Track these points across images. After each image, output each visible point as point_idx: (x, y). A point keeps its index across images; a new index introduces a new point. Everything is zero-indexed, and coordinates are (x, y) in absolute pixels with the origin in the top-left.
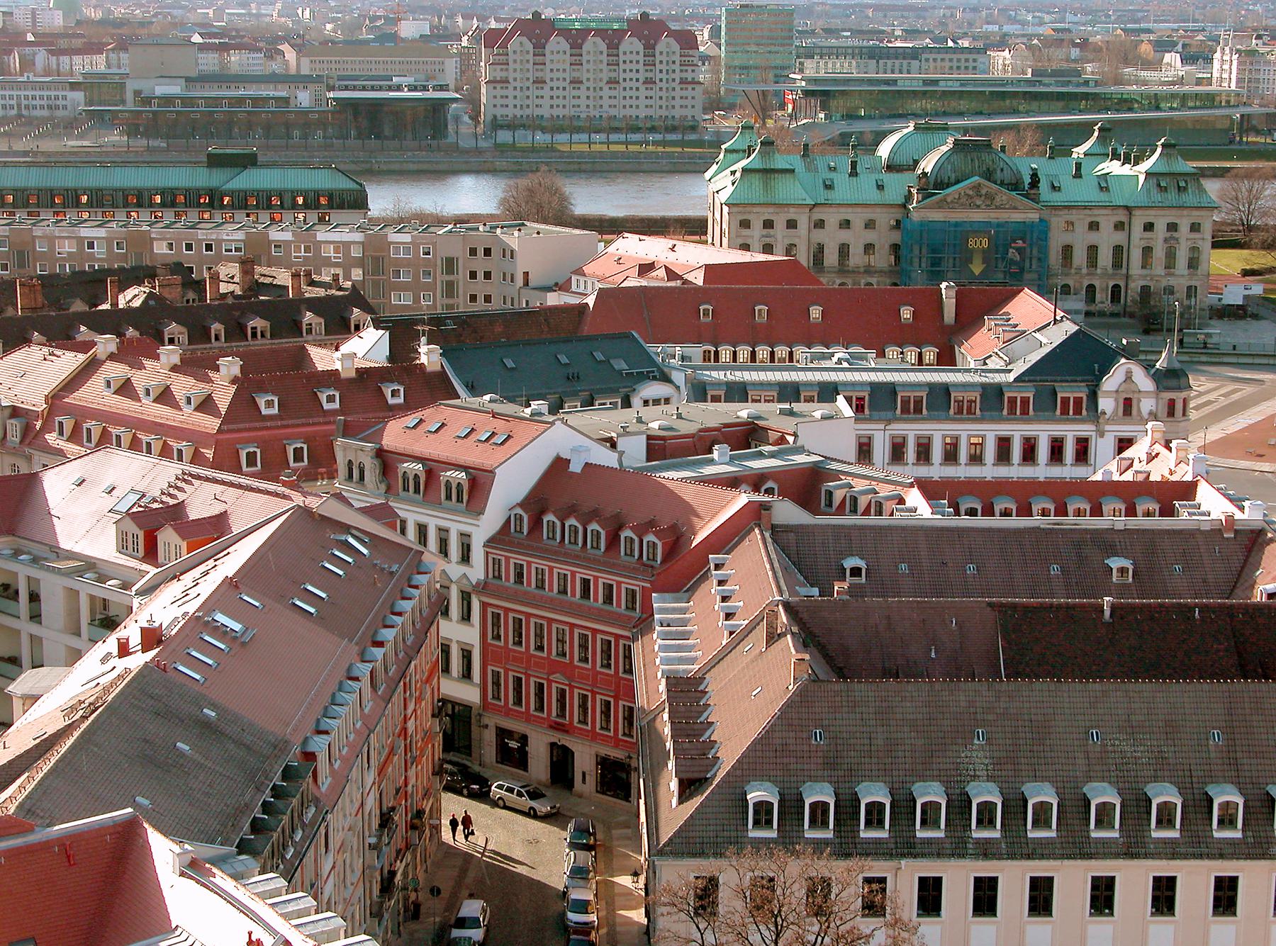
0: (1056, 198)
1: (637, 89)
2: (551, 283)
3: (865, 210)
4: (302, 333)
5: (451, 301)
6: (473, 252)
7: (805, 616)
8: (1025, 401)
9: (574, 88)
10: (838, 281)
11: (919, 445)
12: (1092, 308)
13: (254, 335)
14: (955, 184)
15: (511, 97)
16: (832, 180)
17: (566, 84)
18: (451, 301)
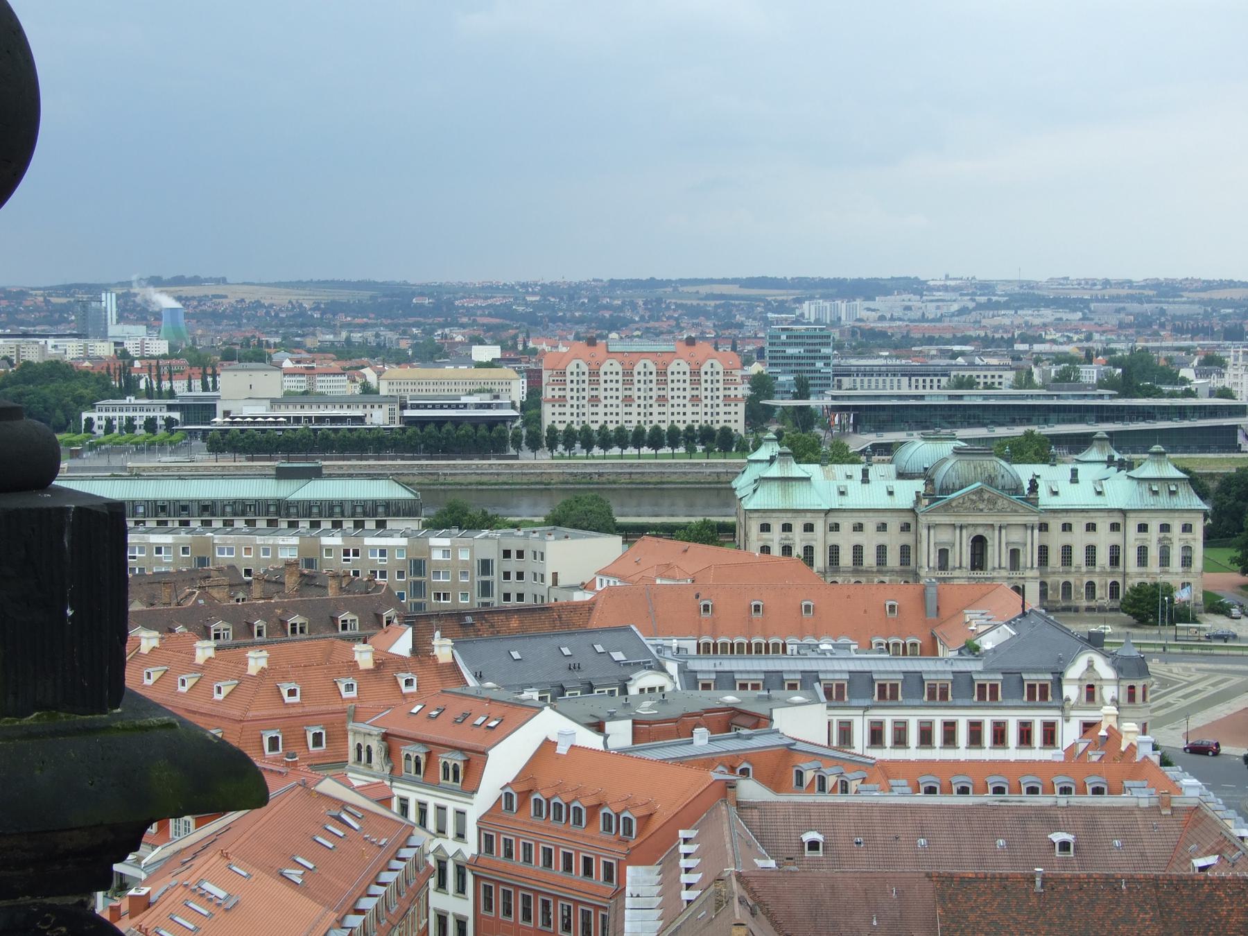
0: (1055, 503)
2: (577, 582)
3: (876, 514)
4: (338, 629)
5: (486, 600)
6: (507, 554)
7: (755, 885)
8: (994, 688)
9: (626, 406)
10: (853, 580)
11: (895, 729)
12: (1092, 604)
13: (294, 631)
14: (959, 489)
16: (846, 487)
17: (619, 402)
18: (486, 600)
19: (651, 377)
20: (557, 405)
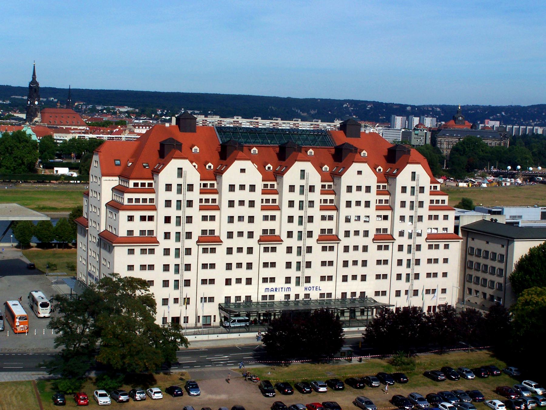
1: (365, 249)
15: (159, 268)
19: (190, 196)
20: (137, 250)
